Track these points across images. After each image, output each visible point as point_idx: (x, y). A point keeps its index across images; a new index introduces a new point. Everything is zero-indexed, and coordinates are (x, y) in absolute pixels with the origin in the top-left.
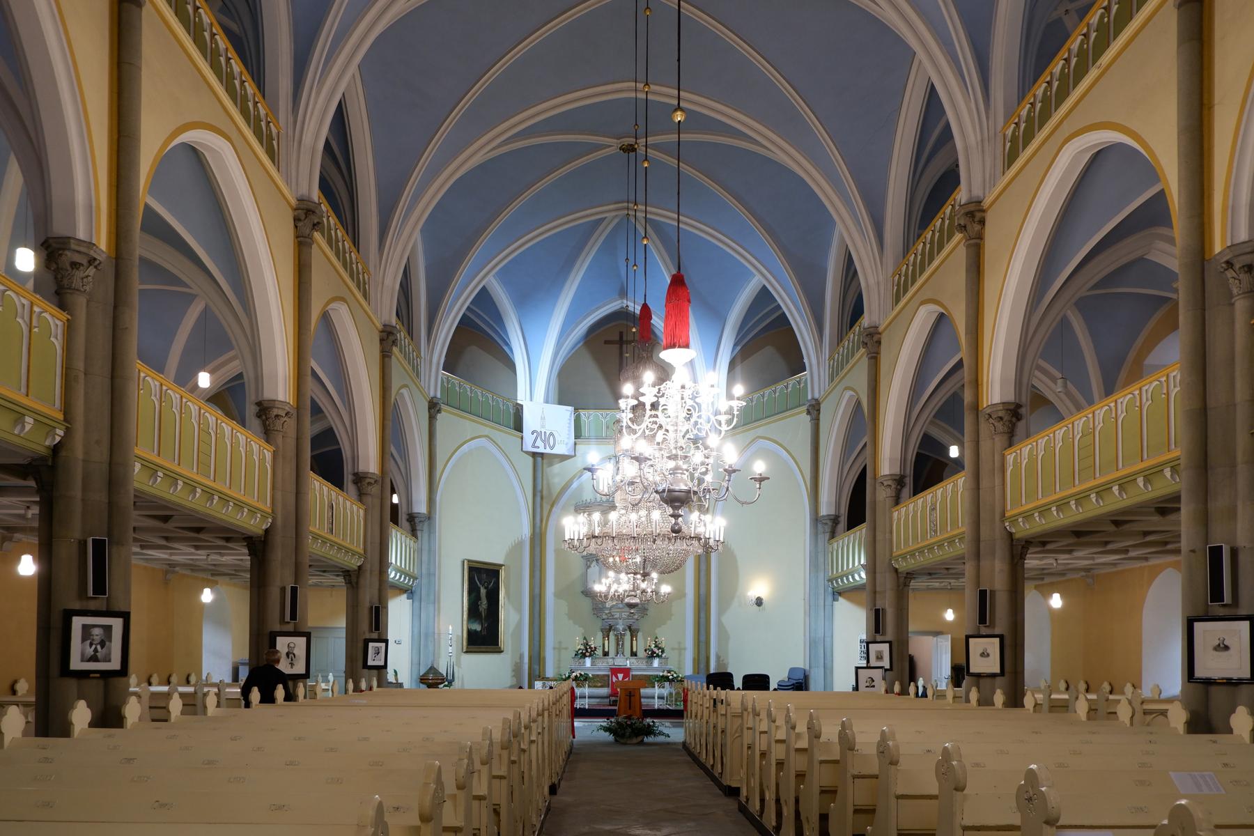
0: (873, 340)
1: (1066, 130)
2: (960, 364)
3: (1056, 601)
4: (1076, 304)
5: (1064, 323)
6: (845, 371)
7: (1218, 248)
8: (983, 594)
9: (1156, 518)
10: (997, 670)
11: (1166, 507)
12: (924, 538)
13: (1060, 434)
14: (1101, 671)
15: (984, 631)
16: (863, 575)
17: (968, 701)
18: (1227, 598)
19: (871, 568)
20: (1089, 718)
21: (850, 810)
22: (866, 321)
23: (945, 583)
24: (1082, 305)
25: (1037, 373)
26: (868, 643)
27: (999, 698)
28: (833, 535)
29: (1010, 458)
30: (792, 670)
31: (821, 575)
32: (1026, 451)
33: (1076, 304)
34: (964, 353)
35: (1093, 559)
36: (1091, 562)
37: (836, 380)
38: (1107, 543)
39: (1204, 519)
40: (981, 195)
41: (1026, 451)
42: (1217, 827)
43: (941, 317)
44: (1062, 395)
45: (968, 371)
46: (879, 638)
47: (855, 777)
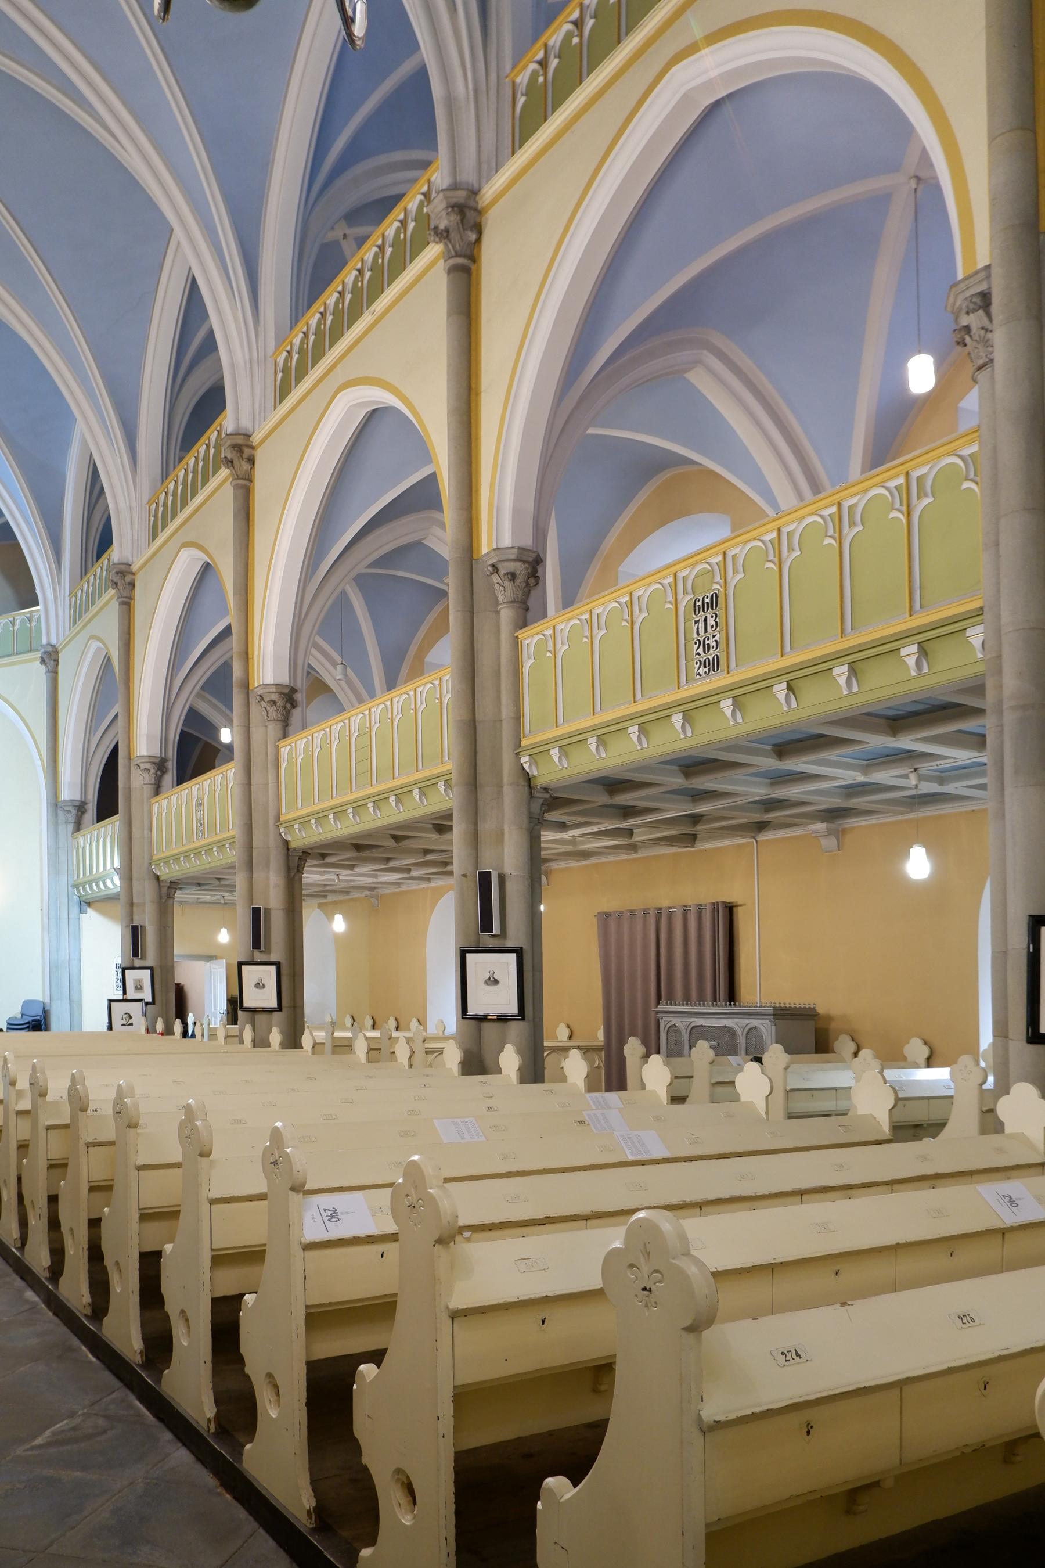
0: (124, 580)
1: (340, 376)
2: (227, 632)
3: (339, 924)
4: (355, 579)
5: (343, 600)
6: (90, 614)
7: (485, 550)
8: (256, 912)
9: (434, 836)
10: (274, 1004)
11: (441, 825)
12: (190, 839)
13: (336, 729)
14: (385, 1005)
15: (259, 957)
16: (117, 880)
17: (242, 1042)
18: (496, 930)
19: (127, 872)
20: (369, 1061)
21: (85, 1187)
22: (115, 554)
23: (217, 896)
24: (361, 581)
25: (314, 651)
26: (124, 970)
27: (275, 1037)
28: (78, 826)
29: (285, 752)
30: (26, 1004)
31: (64, 879)
32: (301, 744)
33: (355, 579)
34: (231, 618)
35: (376, 876)
36: (374, 880)
37: (80, 624)
38: (388, 860)
39: (474, 841)
40: (251, 431)
41: (301, 744)
42: (447, 1180)
43: (207, 567)
44: (343, 684)
45: (233, 639)
46: (138, 963)
47: (89, 1145)
